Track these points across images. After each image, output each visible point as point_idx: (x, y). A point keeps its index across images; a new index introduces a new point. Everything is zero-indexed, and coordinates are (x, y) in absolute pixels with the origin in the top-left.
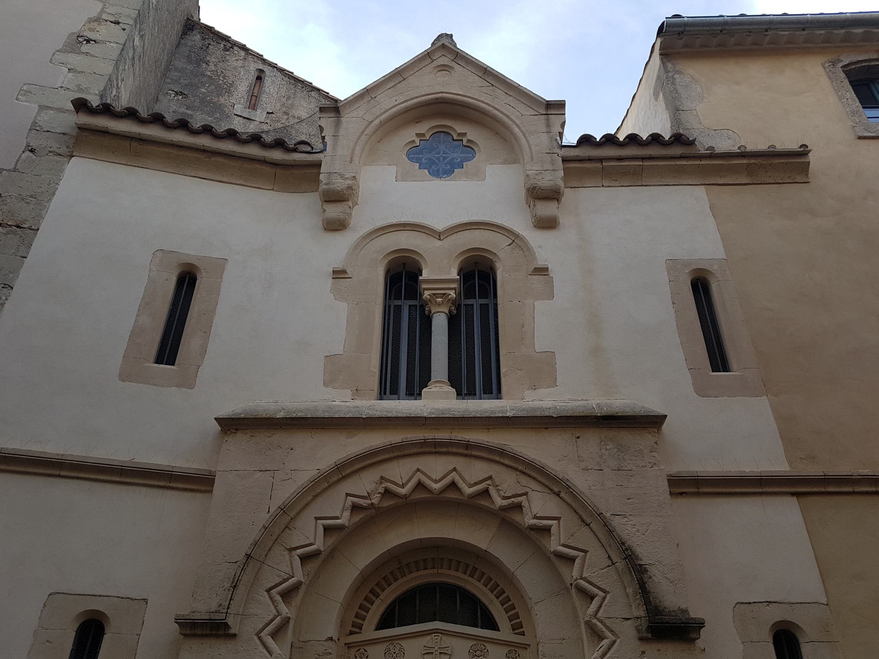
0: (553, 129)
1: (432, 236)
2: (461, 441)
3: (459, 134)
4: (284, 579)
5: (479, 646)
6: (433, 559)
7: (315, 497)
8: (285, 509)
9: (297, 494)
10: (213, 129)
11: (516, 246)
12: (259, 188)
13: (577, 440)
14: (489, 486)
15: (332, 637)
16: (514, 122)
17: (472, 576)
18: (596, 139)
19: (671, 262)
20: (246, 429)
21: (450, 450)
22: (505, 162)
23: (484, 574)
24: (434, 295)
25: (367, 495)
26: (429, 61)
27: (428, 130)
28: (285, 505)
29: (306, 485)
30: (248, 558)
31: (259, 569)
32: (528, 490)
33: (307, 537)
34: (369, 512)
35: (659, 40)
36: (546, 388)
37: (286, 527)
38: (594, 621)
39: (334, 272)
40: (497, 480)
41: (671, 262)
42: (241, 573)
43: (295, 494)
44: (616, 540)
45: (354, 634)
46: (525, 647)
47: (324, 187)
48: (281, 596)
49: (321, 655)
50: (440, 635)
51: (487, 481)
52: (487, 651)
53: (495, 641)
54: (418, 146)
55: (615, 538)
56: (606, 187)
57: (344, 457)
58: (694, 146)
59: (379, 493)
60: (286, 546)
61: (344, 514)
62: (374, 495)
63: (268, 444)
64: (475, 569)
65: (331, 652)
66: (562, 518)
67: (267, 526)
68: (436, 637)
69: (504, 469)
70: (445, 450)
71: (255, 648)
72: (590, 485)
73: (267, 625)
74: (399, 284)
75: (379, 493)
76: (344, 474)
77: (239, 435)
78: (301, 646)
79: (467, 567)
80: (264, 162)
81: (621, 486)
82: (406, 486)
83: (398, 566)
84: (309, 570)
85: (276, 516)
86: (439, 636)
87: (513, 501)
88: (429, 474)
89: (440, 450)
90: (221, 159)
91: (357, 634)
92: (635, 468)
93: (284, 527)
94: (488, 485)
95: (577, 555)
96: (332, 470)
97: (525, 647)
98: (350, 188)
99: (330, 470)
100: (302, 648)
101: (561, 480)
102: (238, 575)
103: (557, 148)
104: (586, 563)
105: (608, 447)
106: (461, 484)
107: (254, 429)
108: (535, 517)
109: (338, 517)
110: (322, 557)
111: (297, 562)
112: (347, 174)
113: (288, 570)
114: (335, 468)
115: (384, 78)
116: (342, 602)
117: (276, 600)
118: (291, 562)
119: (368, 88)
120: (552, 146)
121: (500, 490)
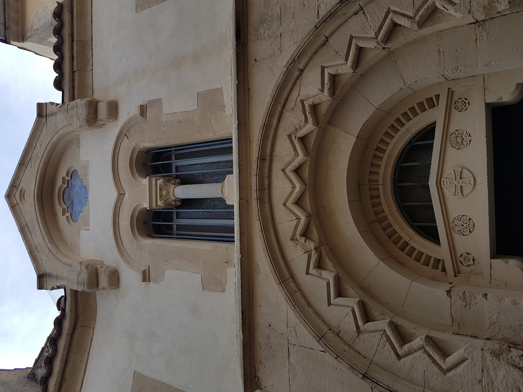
0: (54, 110)
1: (122, 201)
2: (257, 165)
3: (64, 182)
6: (370, 189)
7: (309, 305)
8: (319, 336)
9: (306, 323)
10: (43, 376)
11: (129, 133)
12: (92, 340)
13: (257, 61)
15: (447, 291)
16: (50, 140)
17: (384, 151)
18: (57, 76)
19: (137, 9)
20: (255, 368)
21: (266, 175)
22: (78, 147)
24: (161, 197)
25: (307, 253)
26: (17, 207)
27: (61, 207)
28: (316, 336)
29: (298, 314)
32: (299, 100)
33: (347, 314)
34: (324, 252)
35: (12, 42)
36: (223, 97)
37: (338, 335)
38: (417, 19)
39: (144, 280)
40: (291, 130)
41: (138, 9)
42: (381, 386)
43: (307, 325)
44: (338, 8)
46: (451, 93)
47: (85, 287)
48: (405, 344)
49: (466, 303)
50: (442, 179)
51: (292, 139)
52: (456, 131)
53: (446, 123)
54: (71, 214)
55: (337, 9)
56: (93, 68)
57: (273, 275)
58: (63, 3)
59: (305, 242)
60: (355, 337)
63: (266, 348)
64: (378, 149)
65: (463, 291)
67: (335, 355)
68: (445, 183)
69: (282, 125)
70: (266, 181)
71: (459, 376)
73: (434, 361)
74: (162, 225)
75: (305, 242)
76: (289, 277)
77: (260, 374)
80: (72, 335)
81: (293, 14)
84: (378, 313)
86: (443, 180)
87: (309, 113)
88: (288, 195)
89: (266, 185)
90: (67, 371)
91: (444, 264)
92: (279, 5)
93: (337, 339)
94: (295, 138)
97: (451, 93)
98: (87, 267)
99: (284, 290)
100: (459, 323)
101: (288, 69)
102: (384, 389)
103: (64, 106)
105: (263, 32)
106: (295, 164)
107: (255, 360)
108: (322, 90)
110: (367, 300)
111: (370, 325)
112: (78, 269)
113: (378, 335)
115: (24, 240)
116: (411, 280)
117: (409, 350)
119: (29, 252)
120: (63, 110)
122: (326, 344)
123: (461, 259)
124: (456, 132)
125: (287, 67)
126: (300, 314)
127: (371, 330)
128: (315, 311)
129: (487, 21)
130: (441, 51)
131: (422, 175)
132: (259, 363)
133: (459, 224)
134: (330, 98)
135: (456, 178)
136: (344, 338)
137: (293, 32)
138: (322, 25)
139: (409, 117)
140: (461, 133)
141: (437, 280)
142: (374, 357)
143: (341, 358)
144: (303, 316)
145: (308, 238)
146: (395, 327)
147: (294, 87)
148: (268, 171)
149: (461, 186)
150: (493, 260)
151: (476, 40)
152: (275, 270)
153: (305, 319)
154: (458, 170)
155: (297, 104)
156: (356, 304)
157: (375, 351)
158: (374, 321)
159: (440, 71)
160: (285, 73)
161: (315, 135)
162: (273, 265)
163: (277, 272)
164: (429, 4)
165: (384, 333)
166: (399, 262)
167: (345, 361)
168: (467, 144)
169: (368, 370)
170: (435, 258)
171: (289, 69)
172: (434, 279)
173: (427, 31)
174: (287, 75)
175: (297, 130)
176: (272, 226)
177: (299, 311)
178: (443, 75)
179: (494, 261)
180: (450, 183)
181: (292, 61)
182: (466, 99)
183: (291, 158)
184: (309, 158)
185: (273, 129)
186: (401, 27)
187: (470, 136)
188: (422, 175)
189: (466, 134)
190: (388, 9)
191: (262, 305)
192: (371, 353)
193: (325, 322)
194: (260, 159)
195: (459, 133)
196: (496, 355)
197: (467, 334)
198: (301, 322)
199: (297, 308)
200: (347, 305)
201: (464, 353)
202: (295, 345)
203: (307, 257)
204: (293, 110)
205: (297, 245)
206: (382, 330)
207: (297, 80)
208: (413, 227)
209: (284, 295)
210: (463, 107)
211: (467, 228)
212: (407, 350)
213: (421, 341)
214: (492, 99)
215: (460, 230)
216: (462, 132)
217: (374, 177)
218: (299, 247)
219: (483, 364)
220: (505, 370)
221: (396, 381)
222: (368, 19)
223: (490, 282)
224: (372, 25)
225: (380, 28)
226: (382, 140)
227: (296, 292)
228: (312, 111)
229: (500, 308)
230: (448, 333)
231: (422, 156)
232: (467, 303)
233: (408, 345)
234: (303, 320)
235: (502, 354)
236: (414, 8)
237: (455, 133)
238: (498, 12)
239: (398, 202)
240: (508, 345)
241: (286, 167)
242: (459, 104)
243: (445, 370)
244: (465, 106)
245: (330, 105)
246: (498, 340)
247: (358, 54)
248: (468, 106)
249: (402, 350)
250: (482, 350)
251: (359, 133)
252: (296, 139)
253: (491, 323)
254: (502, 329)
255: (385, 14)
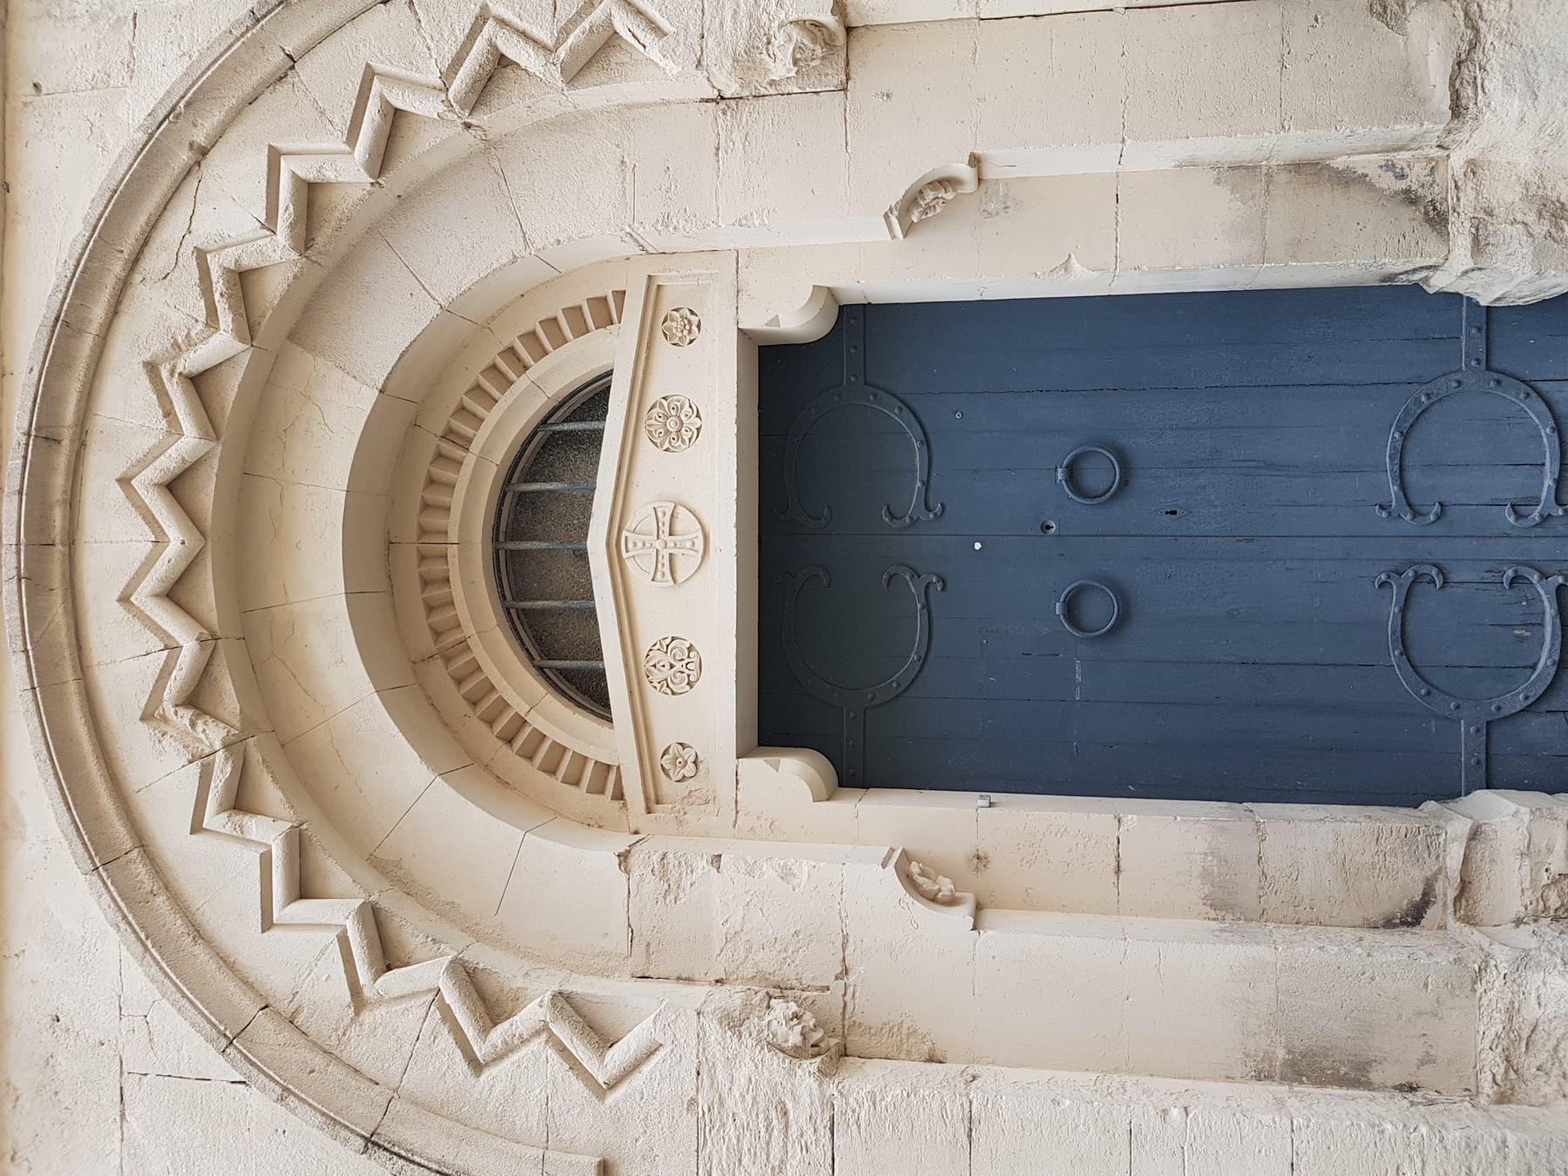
2: (25, 457)
4: (444, 1019)
5: (653, 422)
6: (423, 558)
7: (198, 933)
8: (227, 1033)
9: (184, 996)
13: (44, 91)
14: (178, 371)
15: (619, 856)
23: (463, 408)
28: (214, 1034)
29: (154, 968)
30: (374, 1144)
31: (415, 1103)
32: (188, 249)
33: (322, 952)
34: (256, 757)
37: (292, 1022)
38: (562, 56)
40: (157, 347)
42: (420, 1165)
43: (184, 1001)
45: (621, 787)
46: (654, 291)
48: (495, 1025)
49: (666, 886)
50: (624, 534)
53: (640, 375)
57: (70, 845)
59: (193, 724)
60: (347, 1021)
61: (253, 838)
62: (200, 741)
64: (450, 435)
66: (273, 144)
67: (279, 1090)
68: (630, 545)
69: (123, 325)
72: (180, 53)
73: (574, 1065)
75: (193, 724)
76: (128, 845)
78: (643, 947)
79: (446, 458)
82: (175, 640)
83: (439, 662)
84: (421, 938)
85: (250, 1061)
86: (626, 537)
87: (221, 294)
88: (137, 565)
91: (621, 778)
93: (288, 1035)
95: (377, 100)
96: (109, 882)
97: (654, 291)
99: (109, 891)
100: (648, 945)
101: (151, 136)
104: (402, 73)
106: (169, 462)
109: (262, 855)
110: (389, 901)
111: (394, 980)
113: (417, 1007)
114: (104, 875)
117: (505, 1042)
118: (395, 999)
121: (188, 336)
122: (250, 1056)
123: (666, 761)
124: (663, 401)
125: (150, 131)
126: (161, 968)
127: (396, 995)
128: (218, 954)
129: (746, 101)
130: (628, 163)
131: (575, 522)
132: (8, 1157)
133: (662, 664)
134: (294, 255)
135: (660, 532)
136: (312, 1031)
137: (178, 17)
138: (273, 14)
139: (541, 345)
140: (677, 407)
141: (600, 827)
142: (402, 1077)
143: (296, 1096)
144: (172, 975)
145: (205, 713)
146: (470, 978)
147: (172, 201)
148: (67, 480)
149: (671, 554)
150: (744, 760)
151: (718, 149)
152: (77, 826)
153: (180, 984)
154: (664, 509)
155: (180, 259)
156: (351, 917)
157: (408, 1058)
158: (408, 964)
159: (621, 220)
160: (142, 150)
161: (243, 370)
162: (69, 809)
163: (83, 832)
164: (595, 18)
165: (434, 1000)
166: (498, 777)
167: (310, 1105)
168: (692, 437)
169: (384, 1122)
170: (596, 762)
171: (156, 136)
172: (593, 823)
173: (592, 96)
174: (150, 156)
175: (180, 350)
176: (75, 671)
177: (159, 958)
178: (631, 235)
179: (745, 762)
180: (644, 544)
181: (165, 112)
182: (692, 312)
183: (153, 441)
184: (220, 448)
185: (92, 336)
186: (519, 72)
187: (698, 416)
188: (575, 522)
189: (690, 410)
190: (481, 8)
191: (26, 953)
192: (393, 1068)
193: (248, 984)
194: (36, 436)
195: (671, 407)
196: (733, 1023)
197: (666, 977)
198: (166, 993)
199: (153, 951)
200: (324, 921)
201: (653, 1030)
202: (146, 1075)
203: (198, 775)
204: (169, 277)
205: (163, 735)
206: (430, 990)
207: (185, 178)
208: (545, 673)
209: (109, 907)
210: (685, 332)
211: (682, 672)
212: (499, 1041)
213: (540, 1010)
214: (756, 321)
215: (666, 680)
216: (679, 404)
217: (434, 521)
218: (171, 744)
219: (700, 1055)
220: (753, 1061)
221: (464, 1142)
222: (423, 25)
223: (735, 822)
224: (432, 46)
225: (458, 61)
226: (462, 409)
227: (155, 895)
228: (232, 290)
229: (751, 893)
230: (619, 977)
231: (578, 467)
232: (669, 886)
233: (502, 1027)
234: (174, 989)
235: (748, 1018)
236: (556, 20)
237: (661, 406)
238: (772, 83)
239: (505, 598)
240: (767, 993)
241: (136, 470)
242: (674, 324)
243: (603, 1085)
244: (690, 331)
245: (295, 277)
246: (744, 981)
247: (387, 129)
248: (697, 331)
249: (487, 1042)
250: (698, 1014)
251: (387, 378)
252: (175, 380)
253: (729, 936)
254: (753, 950)
255: (473, 20)
